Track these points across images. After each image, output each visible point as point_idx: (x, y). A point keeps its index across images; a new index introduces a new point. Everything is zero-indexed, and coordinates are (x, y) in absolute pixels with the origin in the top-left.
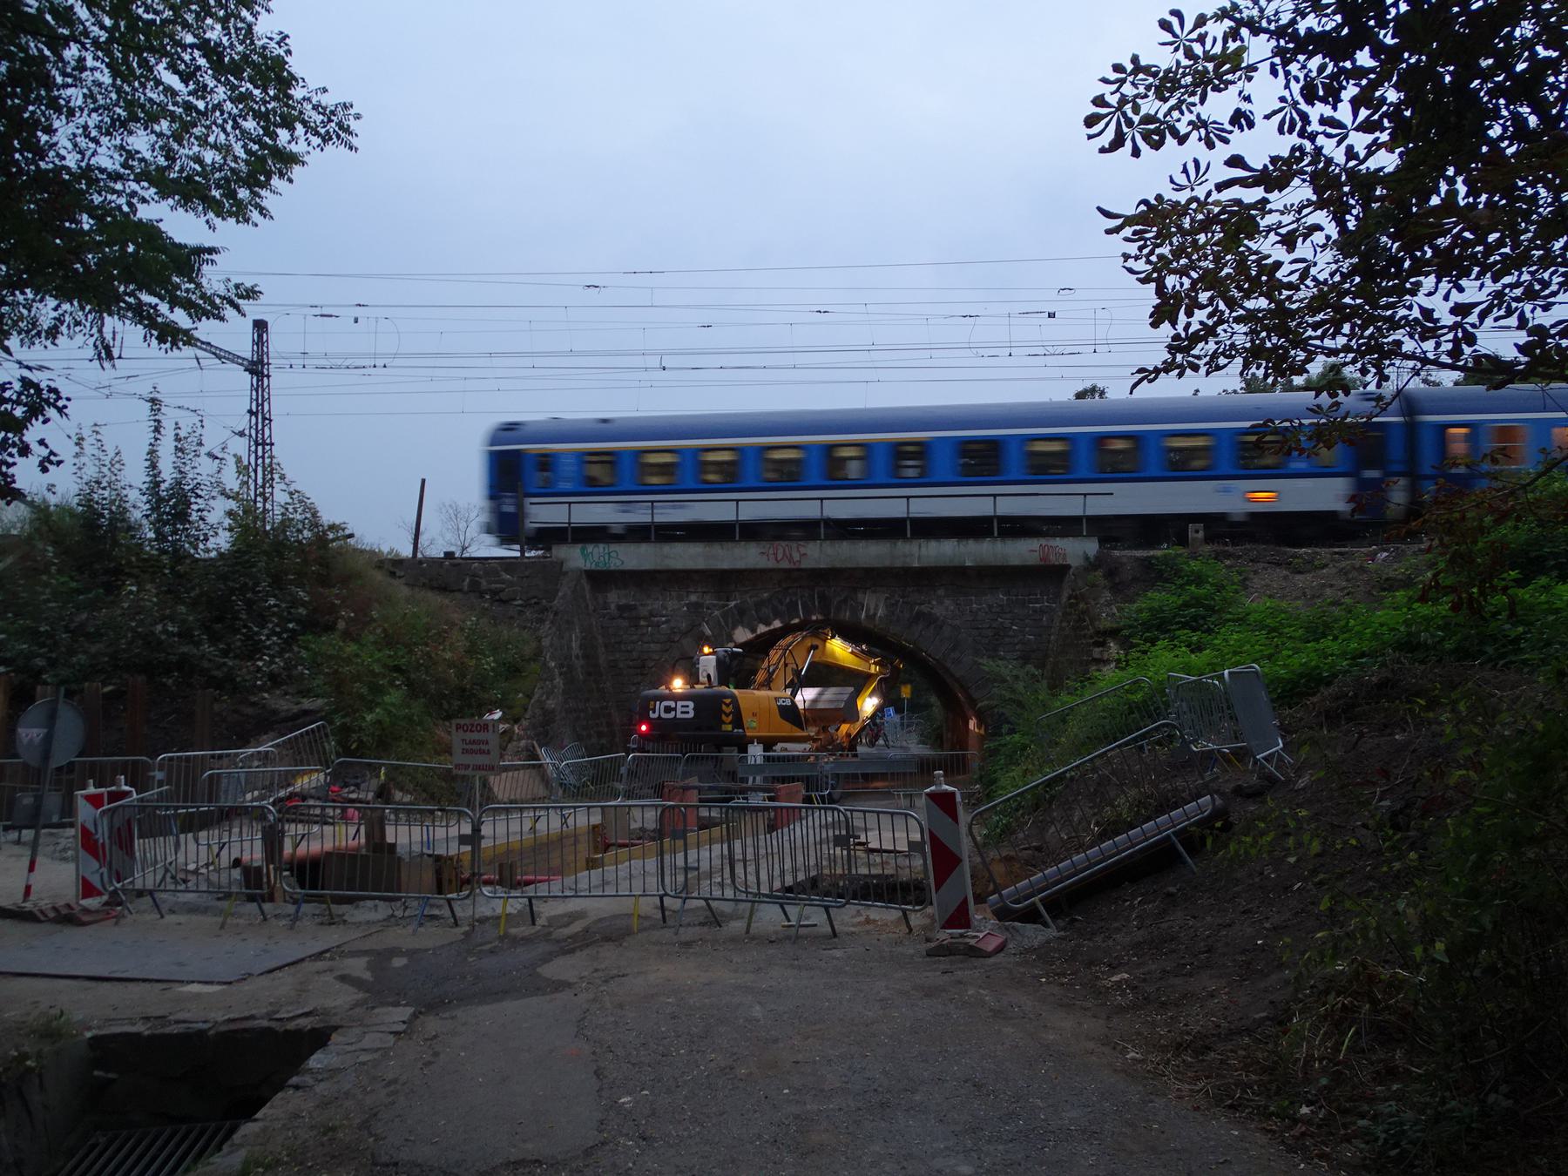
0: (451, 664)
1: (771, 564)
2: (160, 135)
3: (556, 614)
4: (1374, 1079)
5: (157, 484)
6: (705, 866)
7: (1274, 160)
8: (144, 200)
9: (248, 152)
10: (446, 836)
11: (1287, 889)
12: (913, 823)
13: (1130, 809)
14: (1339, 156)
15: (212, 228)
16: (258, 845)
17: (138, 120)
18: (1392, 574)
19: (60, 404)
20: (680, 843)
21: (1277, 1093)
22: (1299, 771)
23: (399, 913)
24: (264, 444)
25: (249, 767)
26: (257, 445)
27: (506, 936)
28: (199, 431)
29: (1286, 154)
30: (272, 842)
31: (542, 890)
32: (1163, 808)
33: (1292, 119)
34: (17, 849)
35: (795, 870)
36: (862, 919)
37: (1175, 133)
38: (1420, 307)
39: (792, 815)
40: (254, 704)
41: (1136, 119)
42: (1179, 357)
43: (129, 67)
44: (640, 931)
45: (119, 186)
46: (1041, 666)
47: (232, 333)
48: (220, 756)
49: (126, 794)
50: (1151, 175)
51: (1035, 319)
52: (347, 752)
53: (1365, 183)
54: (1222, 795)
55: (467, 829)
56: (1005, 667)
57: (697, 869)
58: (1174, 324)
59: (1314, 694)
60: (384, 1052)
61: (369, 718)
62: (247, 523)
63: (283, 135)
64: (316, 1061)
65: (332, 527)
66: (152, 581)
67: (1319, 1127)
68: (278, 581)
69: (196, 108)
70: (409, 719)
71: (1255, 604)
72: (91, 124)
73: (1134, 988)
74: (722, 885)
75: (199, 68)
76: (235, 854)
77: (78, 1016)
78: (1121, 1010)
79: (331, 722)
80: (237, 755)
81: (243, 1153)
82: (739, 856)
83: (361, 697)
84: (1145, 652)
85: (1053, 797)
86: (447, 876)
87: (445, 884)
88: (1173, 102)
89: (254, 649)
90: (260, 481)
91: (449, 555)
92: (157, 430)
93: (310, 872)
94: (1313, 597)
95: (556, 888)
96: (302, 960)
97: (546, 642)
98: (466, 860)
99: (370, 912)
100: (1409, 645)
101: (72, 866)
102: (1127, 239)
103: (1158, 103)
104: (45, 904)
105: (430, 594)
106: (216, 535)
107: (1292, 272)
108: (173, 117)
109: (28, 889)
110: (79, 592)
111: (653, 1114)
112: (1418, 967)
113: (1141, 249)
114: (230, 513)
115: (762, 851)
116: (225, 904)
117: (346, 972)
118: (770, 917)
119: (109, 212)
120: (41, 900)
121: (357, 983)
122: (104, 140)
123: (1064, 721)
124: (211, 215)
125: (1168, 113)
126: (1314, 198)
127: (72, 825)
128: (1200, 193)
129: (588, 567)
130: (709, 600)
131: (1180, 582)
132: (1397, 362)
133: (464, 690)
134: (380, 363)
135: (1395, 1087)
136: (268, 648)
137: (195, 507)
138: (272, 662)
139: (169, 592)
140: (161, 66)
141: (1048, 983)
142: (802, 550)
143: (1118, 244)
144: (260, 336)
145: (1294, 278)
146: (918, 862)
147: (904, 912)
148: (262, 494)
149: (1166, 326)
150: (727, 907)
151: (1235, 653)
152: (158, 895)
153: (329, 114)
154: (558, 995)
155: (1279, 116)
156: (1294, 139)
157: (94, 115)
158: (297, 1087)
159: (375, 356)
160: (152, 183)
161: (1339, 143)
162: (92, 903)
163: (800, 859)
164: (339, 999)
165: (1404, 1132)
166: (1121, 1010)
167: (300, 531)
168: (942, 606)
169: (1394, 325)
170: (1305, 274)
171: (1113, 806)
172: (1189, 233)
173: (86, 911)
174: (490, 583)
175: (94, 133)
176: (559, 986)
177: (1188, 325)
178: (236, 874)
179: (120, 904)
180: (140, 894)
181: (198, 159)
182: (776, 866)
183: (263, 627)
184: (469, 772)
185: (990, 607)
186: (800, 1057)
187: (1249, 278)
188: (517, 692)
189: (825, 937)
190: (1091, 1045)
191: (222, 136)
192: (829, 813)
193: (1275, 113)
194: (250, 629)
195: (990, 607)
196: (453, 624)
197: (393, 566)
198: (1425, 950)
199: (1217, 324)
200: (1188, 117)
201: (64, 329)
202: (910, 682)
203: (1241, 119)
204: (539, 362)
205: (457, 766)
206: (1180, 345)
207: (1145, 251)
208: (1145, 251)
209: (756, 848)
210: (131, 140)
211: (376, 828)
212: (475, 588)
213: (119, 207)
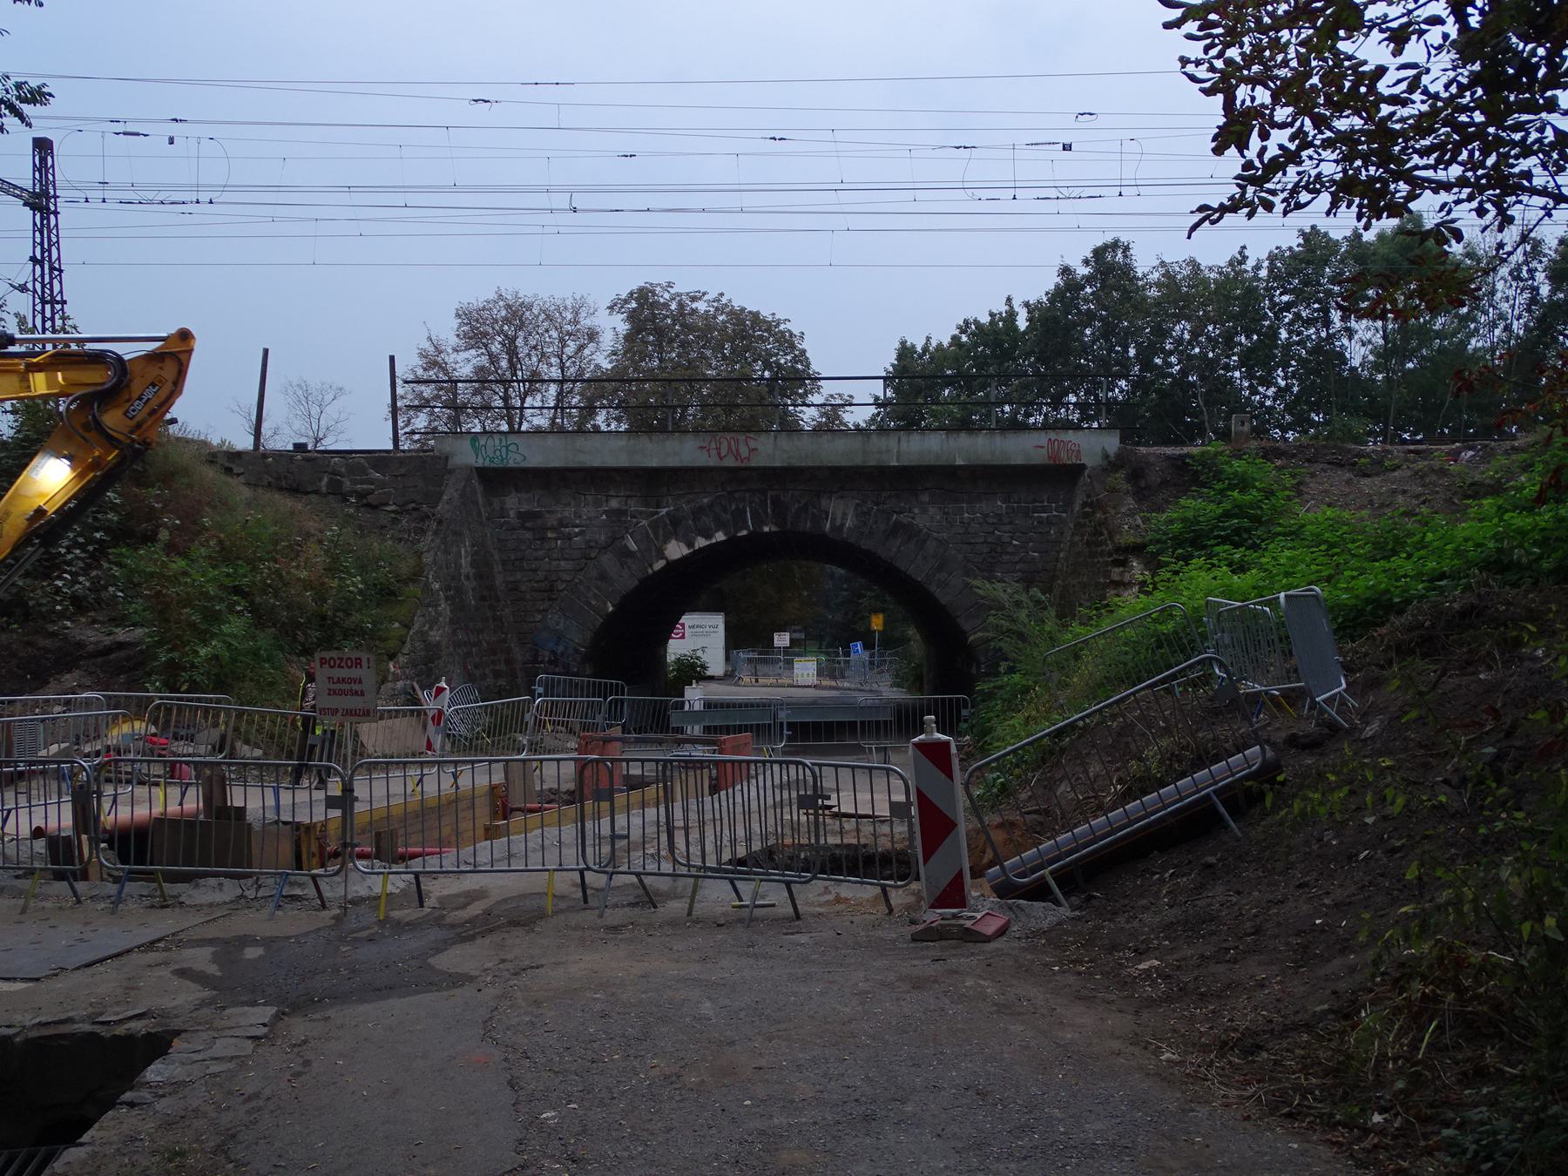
0: (308, 584)
1: (713, 462)
3: (440, 522)
4: (1460, 1081)
6: (636, 834)
10: (305, 804)
11: (1351, 857)
12: (897, 783)
13: (1161, 762)
18: (1478, 478)
20: (605, 805)
21: (1344, 1098)
22: (1366, 717)
23: (251, 894)
24: (53, 302)
26: (44, 302)
27: (387, 919)
30: (85, 815)
31: (433, 863)
32: (1201, 761)
35: (749, 839)
36: (831, 897)
39: (741, 772)
40: (53, 635)
42: (1250, 190)
44: (555, 913)
48: (10, 702)
56: (1002, 590)
57: (627, 837)
59: (1383, 624)
60: (241, 1061)
61: (203, 652)
64: (155, 1073)
67: (1395, 1138)
70: (255, 653)
74: (657, 857)
78: (1151, 1003)
82: (679, 823)
83: (192, 625)
84: (1176, 573)
85: (1063, 750)
86: (308, 848)
91: (300, 447)
93: (134, 844)
94: (1382, 505)
95: (449, 863)
96: (129, 951)
97: (427, 559)
98: (334, 829)
99: (213, 892)
100: (1498, 564)
102: (1190, 37)
107: (1399, 81)
111: (584, 1131)
113: (1207, 49)
115: (708, 816)
116: (25, 884)
117: (185, 965)
118: (717, 895)
123: (1077, 657)
129: (480, 464)
130: (634, 506)
131: (1219, 486)
132: (1525, 198)
133: (324, 618)
134: (204, 197)
136: (69, 563)
138: (75, 582)
141: (1062, 972)
142: (752, 444)
144: (43, 160)
146: (901, 829)
147: (884, 889)
149: (1232, 151)
150: (662, 884)
154: (457, 991)
158: (132, 1105)
159: (198, 187)
163: (756, 827)
164: (183, 998)
165: (1498, 1142)
166: (1151, 1003)
168: (926, 516)
171: (1140, 759)
174: (354, 482)
177: (1264, 150)
178: (40, 845)
182: (726, 832)
185: (986, 516)
186: (763, 1062)
188: (391, 620)
189: (786, 919)
190: (1116, 1045)
192: (792, 768)
195: (986, 516)
196: (308, 535)
197: (229, 460)
199: (1301, 148)
202: (883, 611)
204: (413, 199)
206: (1256, 177)
207: (1213, 52)
209: (701, 812)
211: (215, 790)
212: (336, 490)
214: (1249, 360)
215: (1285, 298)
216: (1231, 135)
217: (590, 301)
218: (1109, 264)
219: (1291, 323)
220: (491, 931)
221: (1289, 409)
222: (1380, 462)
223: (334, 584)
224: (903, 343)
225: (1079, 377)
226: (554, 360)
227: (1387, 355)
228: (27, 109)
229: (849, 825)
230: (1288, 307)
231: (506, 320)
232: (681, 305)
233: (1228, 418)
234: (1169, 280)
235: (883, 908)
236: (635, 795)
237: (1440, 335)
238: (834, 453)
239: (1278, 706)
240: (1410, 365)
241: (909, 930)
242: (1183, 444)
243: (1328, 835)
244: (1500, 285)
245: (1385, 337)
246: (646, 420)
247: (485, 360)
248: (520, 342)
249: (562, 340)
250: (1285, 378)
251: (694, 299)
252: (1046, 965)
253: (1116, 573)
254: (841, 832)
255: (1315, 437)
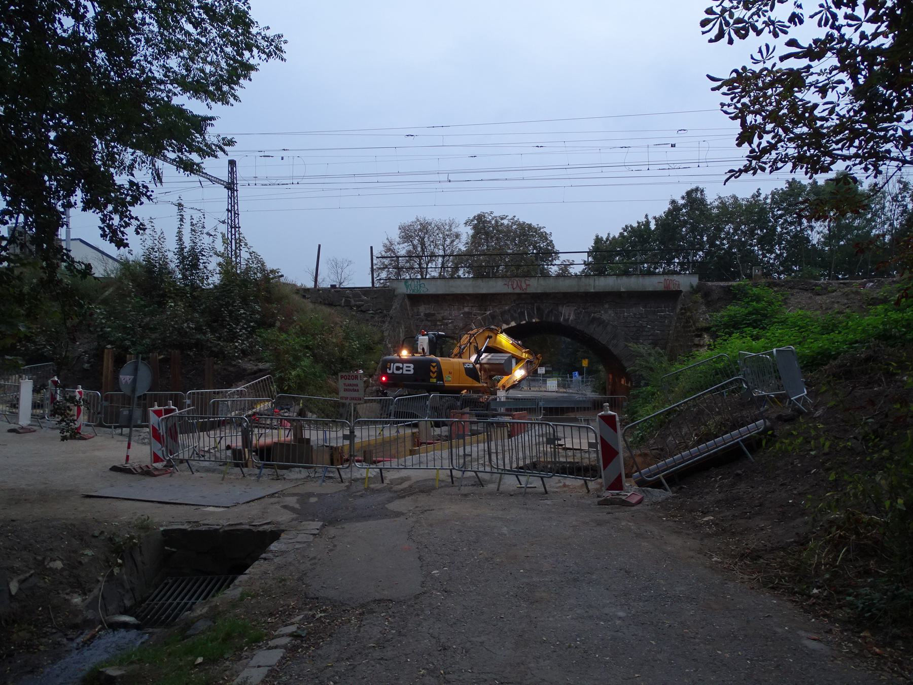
1: (510, 290)
2: (183, 58)
3: (391, 318)
5: (182, 249)
6: (474, 455)
7: (816, 41)
8: (175, 94)
9: (228, 65)
10: (336, 437)
12: (592, 435)
14: (856, 40)
15: (210, 107)
16: (240, 438)
17: (171, 50)
18: (875, 296)
19: (148, 194)
20: (461, 441)
21: (800, 581)
22: (816, 407)
23: (312, 475)
24: (235, 227)
25: (233, 398)
26: (232, 228)
27: (368, 488)
28: (203, 220)
29: (823, 37)
31: (387, 465)
33: (827, 17)
34: (121, 438)
35: (524, 458)
36: (561, 485)
37: (755, 29)
38: (902, 129)
40: (234, 366)
41: (731, 21)
42: (754, 162)
43: (167, 22)
45: (162, 87)
46: (664, 348)
47: (216, 166)
48: (218, 393)
49: (173, 410)
50: (741, 54)
51: (660, 149)
52: (283, 391)
53: (870, 55)
54: (770, 420)
55: (347, 432)
56: (643, 348)
58: (750, 143)
59: (826, 365)
62: (227, 268)
63: (247, 54)
64: (274, 547)
65: (272, 271)
66: (181, 300)
67: (824, 600)
68: (245, 300)
69: (201, 42)
70: (315, 374)
71: (791, 313)
72: (148, 54)
73: (716, 525)
74: (484, 465)
75: (203, 20)
76: (228, 443)
77: (156, 520)
78: (709, 536)
79: (274, 376)
80: (226, 392)
81: (240, 589)
82: (493, 450)
83: (289, 362)
85: (670, 421)
86: (336, 457)
87: (335, 461)
88: (754, 10)
89: (233, 337)
90: (234, 248)
91: (333, 286)
92: (181, 220)
93: (266, 453)
94: (827, 309)
95: (394, 465)
97: (386, 334)
98: (346, 449)
99: (297, 474)
100: (885, 337)
101: (148, 447)
102: (724, 94)
103: (744, 11)
104: (136, 465)
105: (323, 307)
106: (212, 274)
107: (824, 110)
108: (189, 48)
109: (128, 457)
110: (145, 306)
112: (887, 513)
113: (732, 99)
114: (219, 264)
115: (506, 448)
116: (223, 468)
118: (510, 482)
119: (158, 101)
120: (134, 463)
121: (292, 509)
122: (155, 62)
123: (677, 379)
124: (209, 100)
125: (751, 17)
126: (839, 65)
127: (147, 426)
128: (769, 65)
130: (475, 310)
132: (887, 162)
133: (343, 359)
134: (295, 181)
135: (869, 580)
137: (201, 261)
138: (243, 343)
139: (190, 306)
140: (183, 20)
141: (667, 520)
142: (528, 282)
143: (720, 97)
144: (232, 169)
145: (825, 114)
146: (593, 456)
147: (585, 481)
148: (236, 253)
149: (746, 145)
151: (779, 341)
152: (191, 462)
153: (270, 41)
155: (819, 16)
156: (827, 29)
157: (150, 49)
158: (265, 559)
159: (293, 177)
160: (179, 85)
161: (856, 30)
162: (159, 465)
164: (284, 517)
166: (709, 536)
167: (255, 273)
168: (607, 314)
169: (887, 140)
170: (832, 111)
172: (760, 89)
173: (156, 469)
175: (149, 59)
176: (398, 514)
177: (760, 144)
178: (229, 453)
179: (172, 467)
180: (181, 461)
181: (202, 71)
183: (237, 325)
184: (347, 402)
185: (635, 314)
186: (529, 554)
187: (797, 115)
188: (371, 360)
190: (691, 553)
191: (215, 57)
193: (816, 14)
194: (231, 326)
195: (635, 314)
196: (336, 324)
197: (304, 292)
198: (891, 503)
200: (763, 19)
201: (136, 165)
203: (796, 19)
205: (342, 398)
206: (755, 156)
207: (735, 100)
208: (735, 100)
209: (503, 446)
210: (168, 61)
211: (298, 431)
212: (348, 305)
213: (163, 98)
214: (762, 241)
215: (780, 212)
216: (745, 137)
217: (457, 221)
218: (694, 199)
219: (783, 224)
220: (412, 494)
221: (781, 264)
222: (826, 289)
223: (347, 344)
224: (597, 236)
225: (679, 251)
226: (441, 247)
227: (830, 238)
228: (226, 148)
229: (570, 453)
230: (781, 216)
231: (420, 230)
232: (497, 222)
233: (751, 269)
234: (723, 206)
235: (585, 490)
236: (474, 438)
237: (857, 228)
238: (564, 286)
239: (774, 402)
240: (842, 243)
241: (596, 500)
242: (730, 280)
243: (796, 462)
244: (887, 204)
245: (829, 230)
246: (480, 273)
247: (411, 248)
248: (426, 239)
249: (444, 238)
250: (780, 250)
251: (502, 219)
252: (660, 517)
253: (696, 340)
254: (566, 457)
255: (794, 277)
